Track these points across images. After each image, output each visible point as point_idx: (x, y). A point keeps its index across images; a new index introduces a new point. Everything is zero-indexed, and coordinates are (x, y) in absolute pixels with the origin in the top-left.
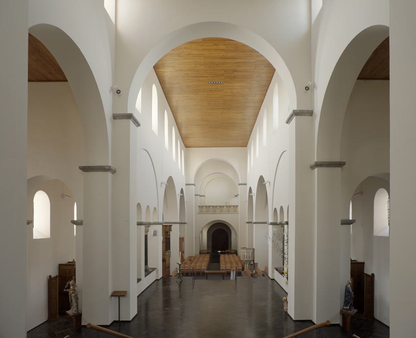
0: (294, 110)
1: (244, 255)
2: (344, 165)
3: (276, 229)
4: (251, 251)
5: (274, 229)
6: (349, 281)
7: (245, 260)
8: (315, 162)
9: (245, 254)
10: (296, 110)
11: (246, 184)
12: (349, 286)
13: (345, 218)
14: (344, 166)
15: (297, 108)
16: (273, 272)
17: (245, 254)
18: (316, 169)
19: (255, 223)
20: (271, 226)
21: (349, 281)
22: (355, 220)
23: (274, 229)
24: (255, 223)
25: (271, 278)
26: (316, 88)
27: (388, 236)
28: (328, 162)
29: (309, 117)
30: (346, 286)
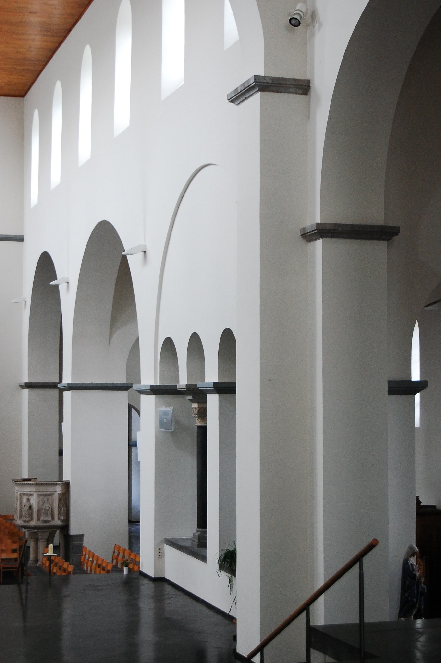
0: (256, 77)
1: (30, 508)
2: (397, 234)
3: (170, 409)
4: (59, 489)
5: (164, 408)
6: (411, 548)
7: (34, 523)
8: (317, 224)
9: (34, 501)
10: (264, 77)
11: (20, 239)
12: (413, 560)
13: (397, 376)
14: (396, 238)
15: (265, 72)
16: (160, 554)
17: (34, 501)
18: (319, 243)
19: (72, 387)
20: (152, 398)
21: (411, 548)
22: (426, 382)
23: (164, 408)
24: (72, 387)
25: (152, 574)
26: (321, 25)
27: (58, 545)
28: (352, 226)
29: (298, 96)
30: (406, 562)
